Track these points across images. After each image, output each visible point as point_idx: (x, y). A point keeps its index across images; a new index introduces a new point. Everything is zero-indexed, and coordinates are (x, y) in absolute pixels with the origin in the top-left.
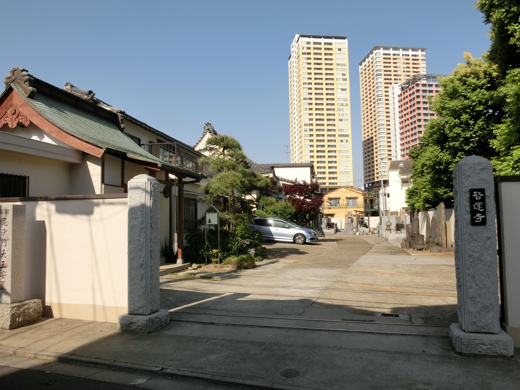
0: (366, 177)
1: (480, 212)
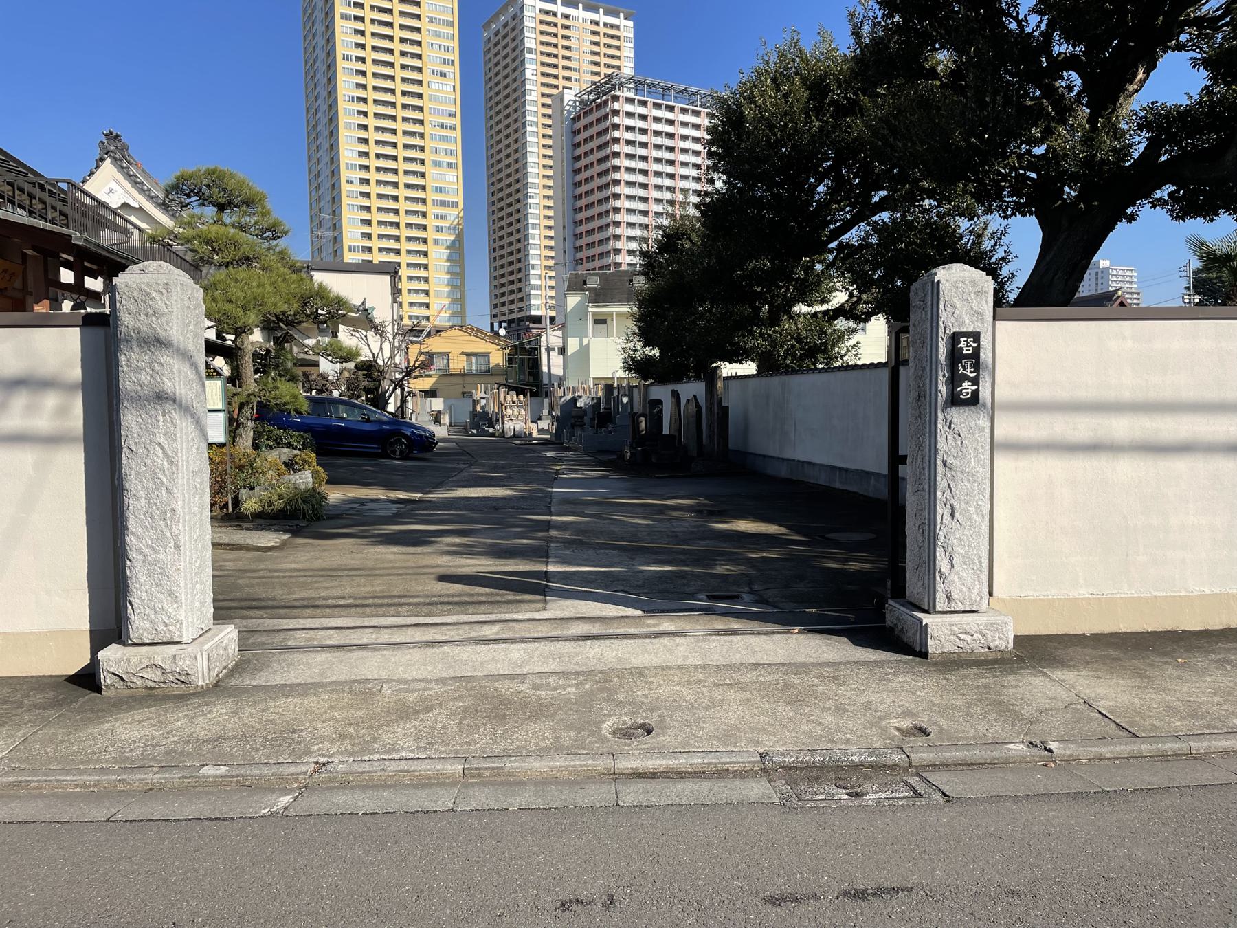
0: (495, 306)
1: (969, 379)
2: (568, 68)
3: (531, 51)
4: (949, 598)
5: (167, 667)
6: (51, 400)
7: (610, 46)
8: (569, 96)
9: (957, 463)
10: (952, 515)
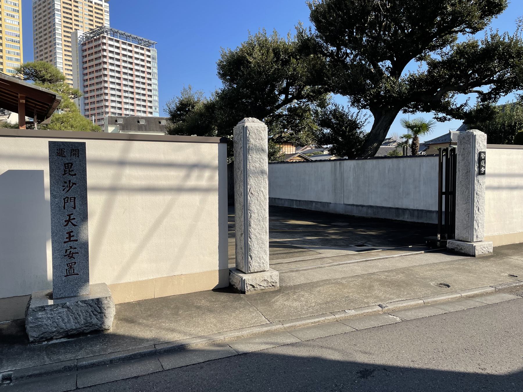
2: (77, 21)
3: (58, 10)
4: (477, 237)
5: (269, 280)
6: (207, 174)
7: (98, 13)
8: (80, 33)
9: (480, 193)
10: (478, 210)
